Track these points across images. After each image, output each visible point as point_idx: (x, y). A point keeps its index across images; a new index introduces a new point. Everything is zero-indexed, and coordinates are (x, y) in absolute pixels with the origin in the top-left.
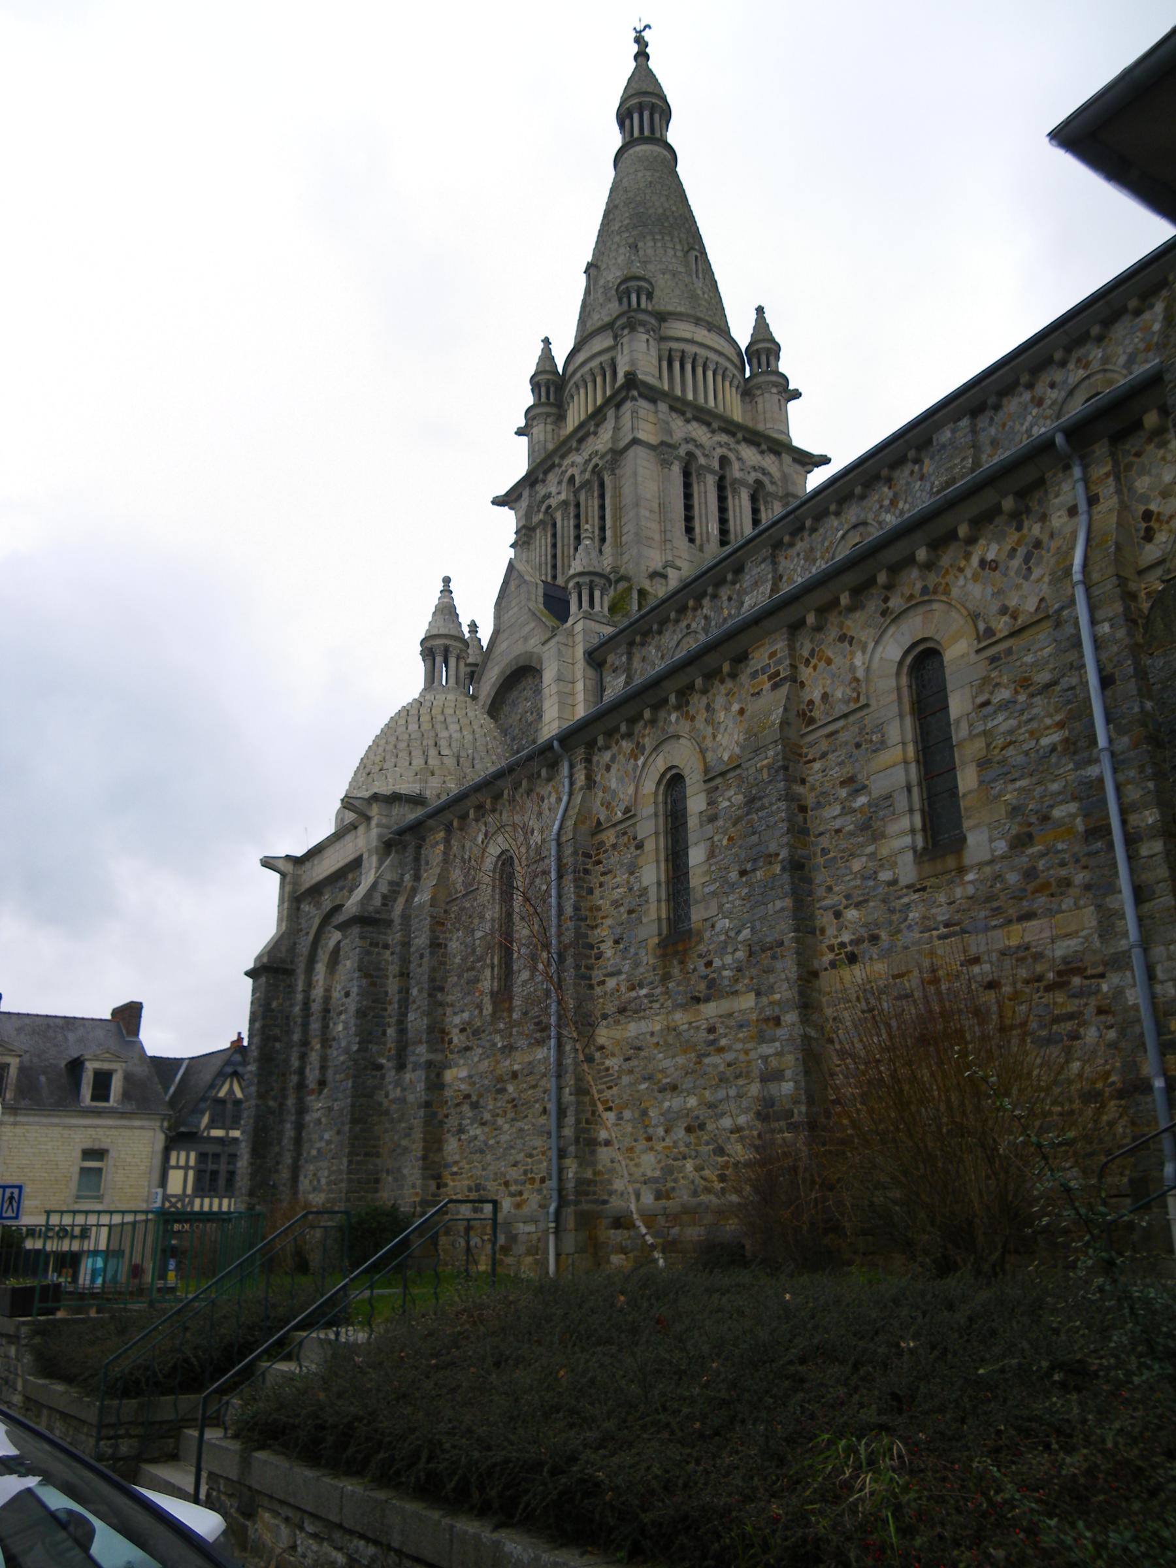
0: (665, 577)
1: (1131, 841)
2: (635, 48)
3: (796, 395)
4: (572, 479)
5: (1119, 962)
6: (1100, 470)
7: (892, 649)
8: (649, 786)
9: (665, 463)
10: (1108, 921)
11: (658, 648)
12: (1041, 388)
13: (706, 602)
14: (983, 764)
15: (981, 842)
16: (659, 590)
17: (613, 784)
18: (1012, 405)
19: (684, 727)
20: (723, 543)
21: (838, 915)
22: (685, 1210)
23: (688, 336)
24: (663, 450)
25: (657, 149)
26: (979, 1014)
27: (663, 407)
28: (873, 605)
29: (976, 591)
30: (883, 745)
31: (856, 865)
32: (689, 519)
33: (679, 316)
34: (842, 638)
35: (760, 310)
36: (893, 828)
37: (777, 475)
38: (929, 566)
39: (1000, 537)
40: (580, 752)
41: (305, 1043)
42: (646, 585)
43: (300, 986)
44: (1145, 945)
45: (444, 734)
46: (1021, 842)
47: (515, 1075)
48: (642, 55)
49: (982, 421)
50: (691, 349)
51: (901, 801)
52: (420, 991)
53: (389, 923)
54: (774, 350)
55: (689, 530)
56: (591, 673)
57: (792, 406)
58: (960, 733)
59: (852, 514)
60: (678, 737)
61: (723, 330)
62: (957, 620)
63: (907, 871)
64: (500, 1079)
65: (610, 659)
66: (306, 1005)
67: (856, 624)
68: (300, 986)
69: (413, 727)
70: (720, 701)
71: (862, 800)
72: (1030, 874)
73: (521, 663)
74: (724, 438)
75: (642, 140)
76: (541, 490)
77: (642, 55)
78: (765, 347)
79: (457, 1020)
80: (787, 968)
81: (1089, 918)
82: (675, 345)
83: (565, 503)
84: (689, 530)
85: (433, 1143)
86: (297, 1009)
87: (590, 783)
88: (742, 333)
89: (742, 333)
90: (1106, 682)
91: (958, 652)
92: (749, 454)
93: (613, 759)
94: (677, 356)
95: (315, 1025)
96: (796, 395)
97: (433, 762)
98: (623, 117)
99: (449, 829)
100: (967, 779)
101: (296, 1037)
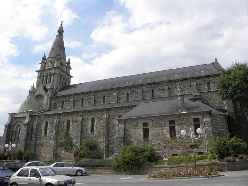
1: (106, 136)
2: (61, 23)
4: (47, 73)
5: (104, 142)
6: (107, 111)
7: (91, 117)
8: (66, 120)
9: (59, 76)
10: (103, 140)
12: (101, 93)
14: (97, 127)
15: (96, 132)
17: (62, 119)
18: (98, 93)
19: (71, 116)
21: (84, 135)
22: (67, 156)
24: (59, 75)
25: (61, 37)
26: (137, 161)
27: (60, 70)
28: (90, 113)
29: (98, 115)
32: (60, 82)
33: (62, 59)
37: (68, 78)
38: (95, 112)
40: (59, 115)
41: (12, 135)
43: (12, 128)
44: (105, 142)
45: (34, 103)
46: (98, 133)
47: (47, 143)
48: (62, 24)
49: (96, 93)
50: (63, 63)
51: (90, 128)
53: (30, 125)
55: (60, 83)
59: (83, 96)
62: (96, 117)
63: (90, 133)
66: (13, 131)
67: (88, 114)
68: (12, 128)
70: (74, 115)
72: (99, 136)
74: (64, 73)
75: (60, 35)
76: (42, 73)
77: (62, 24)
78: (69, 63)
79: (38, 136)
80: (79, 139)
81: (102, 139)
83: (46, 76)
84: (60, 83)
85: (35, 148)
86: (11, 131)
87: (59, 118)
88: (67, 60)
89: (67, 60)
90: (106, 126)
92: (66, 75)
95: (14, 133)
98: (58, 31)
100: (95, 128)
101: (11, 134)
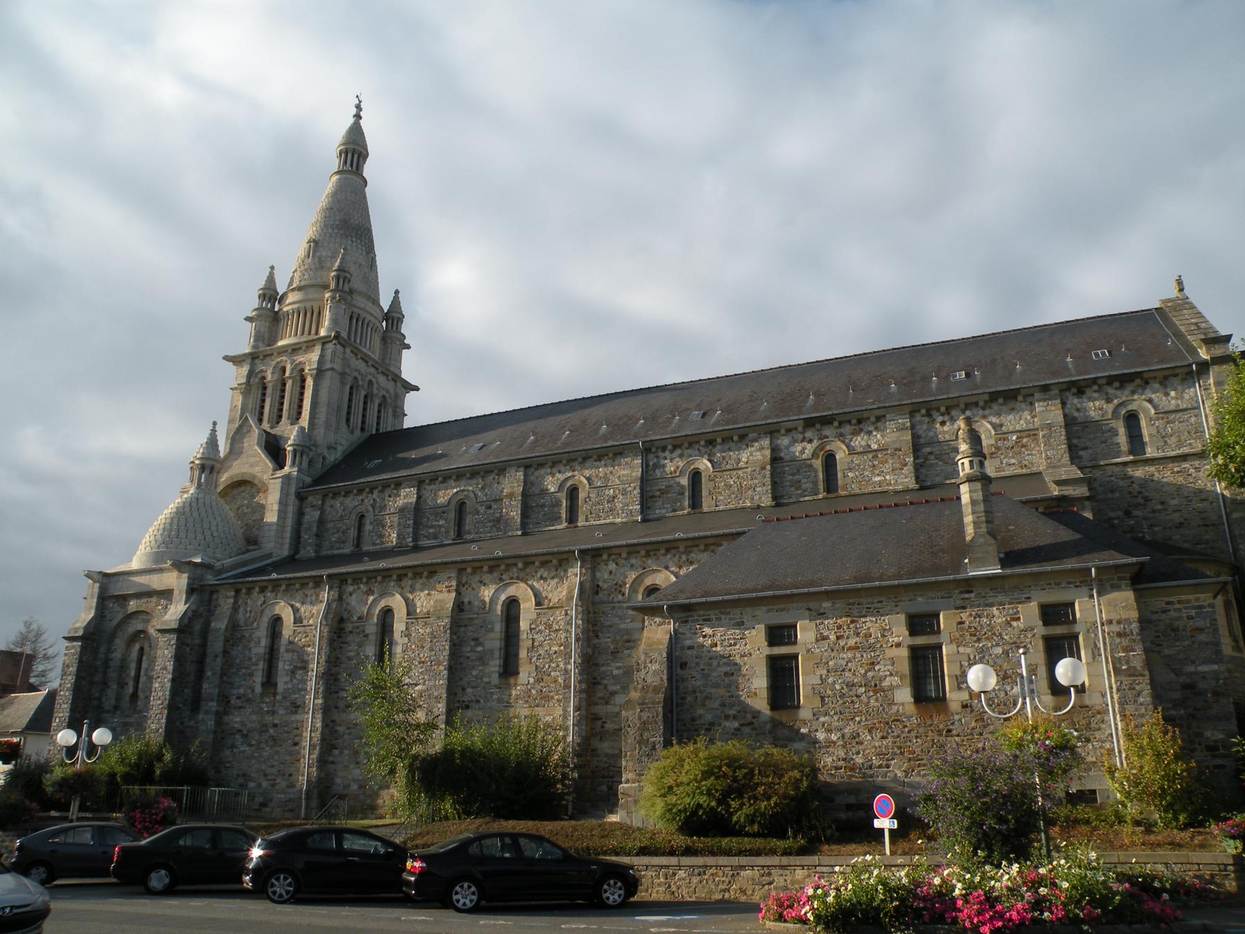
0: (335, 449)
3: (408, 347)
11: (342, 504)
13: (376, 492)
16: (332, 457)
17: (353, 603)
20: (363, 429)
21: (464, 689)
23: (362, 306)
30: (492, 630)
31: (474, 673)
34: (481, 582)
35: (397, 292)
36: (492, 663)
37: (392, 392)
39: (549, 571)
42: (326, 453)
47: (275, 725)
48: (358, 117)
51: (497, 654)
52: (214, 674)
54: (400, 319)
55: (348, 420)
56: (297, 502)
57: (404, 351)
58: (523, 636)
60: (755, 908)
61: (376, 302)
64: (265, 725)
65: (310, 499)
69: (196, 514)
71: (480, 649)
73: (246, 478)
77: (358, 117)
78: (394, 317)
82: (356, 310)
84: (348, 420)
88: (385, 304)
89: (385, 304)
91: (527, 609)
93: (354, 591)
94: (355, 316)
96: (408, 347)
97: (209, 538)
99: (238, 591)
